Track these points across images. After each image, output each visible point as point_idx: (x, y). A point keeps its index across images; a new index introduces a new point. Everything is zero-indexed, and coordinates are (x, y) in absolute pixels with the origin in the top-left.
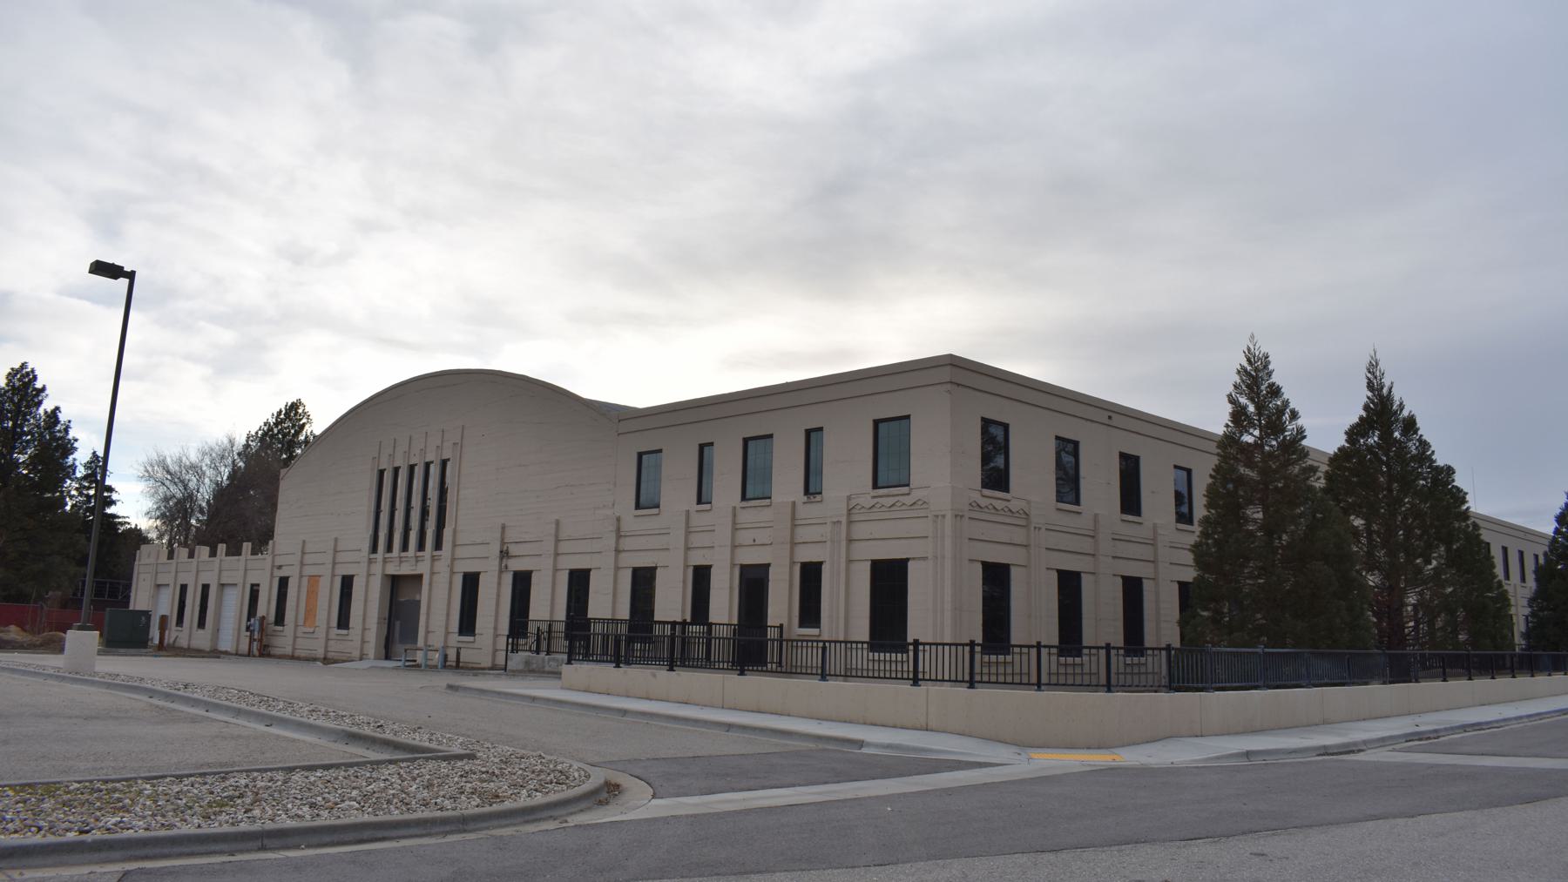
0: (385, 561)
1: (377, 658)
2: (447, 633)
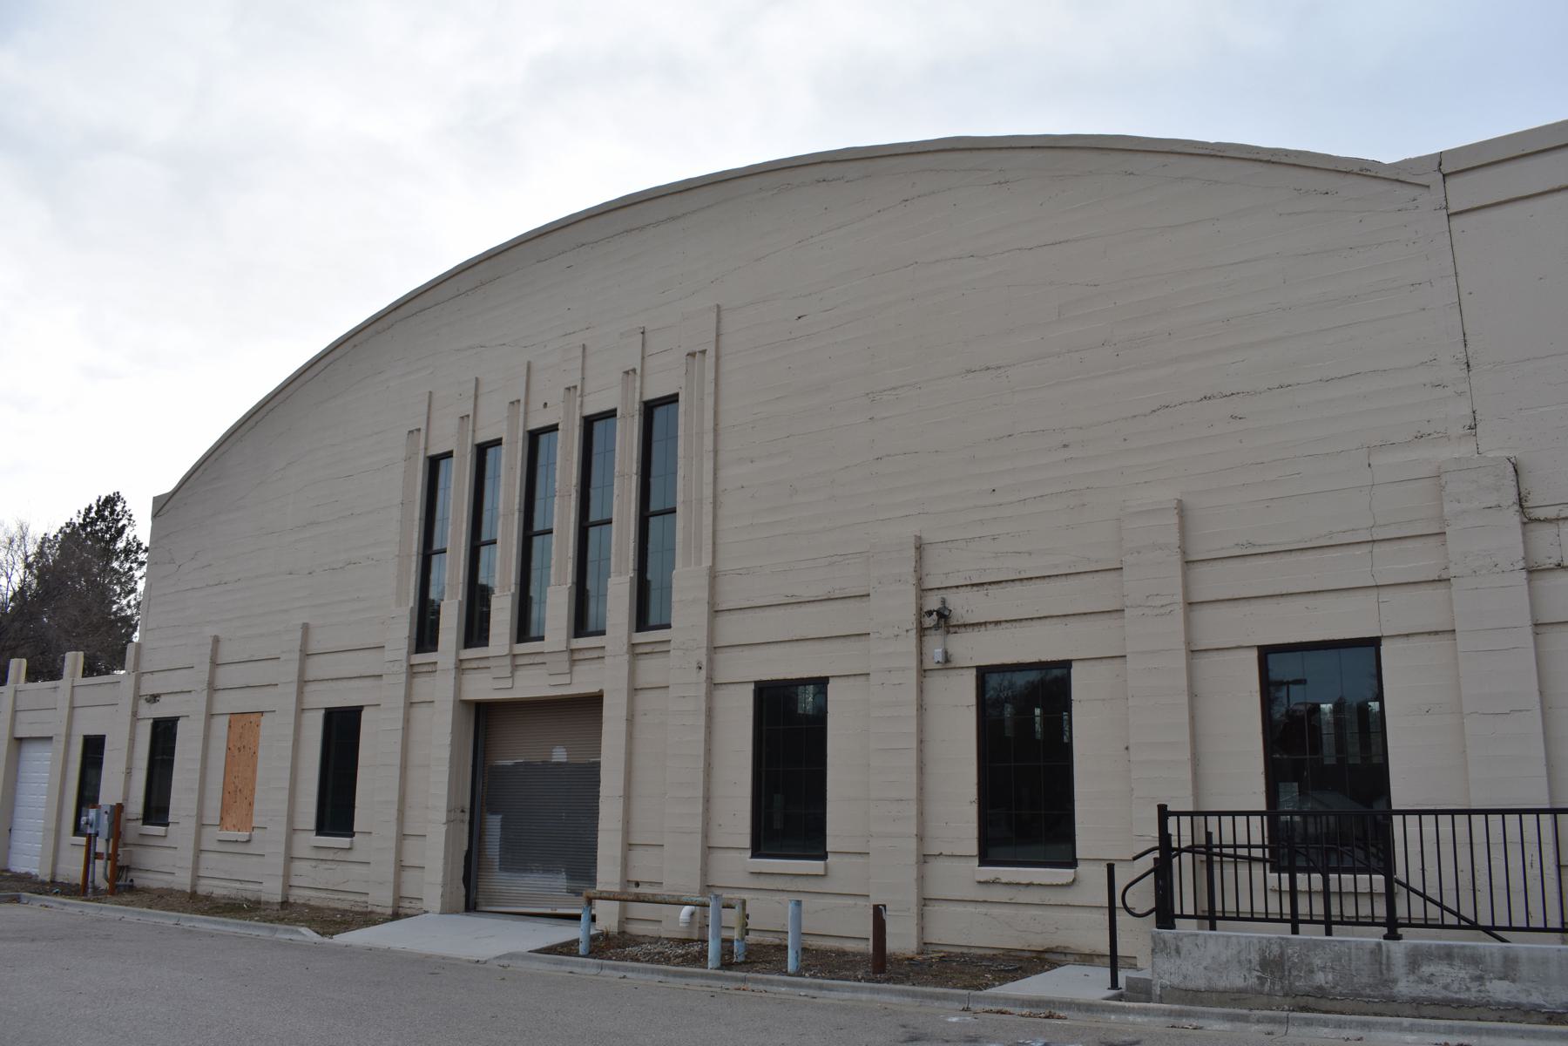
0: (460, 667)
1: (447, 910)
2: (292, 831)
